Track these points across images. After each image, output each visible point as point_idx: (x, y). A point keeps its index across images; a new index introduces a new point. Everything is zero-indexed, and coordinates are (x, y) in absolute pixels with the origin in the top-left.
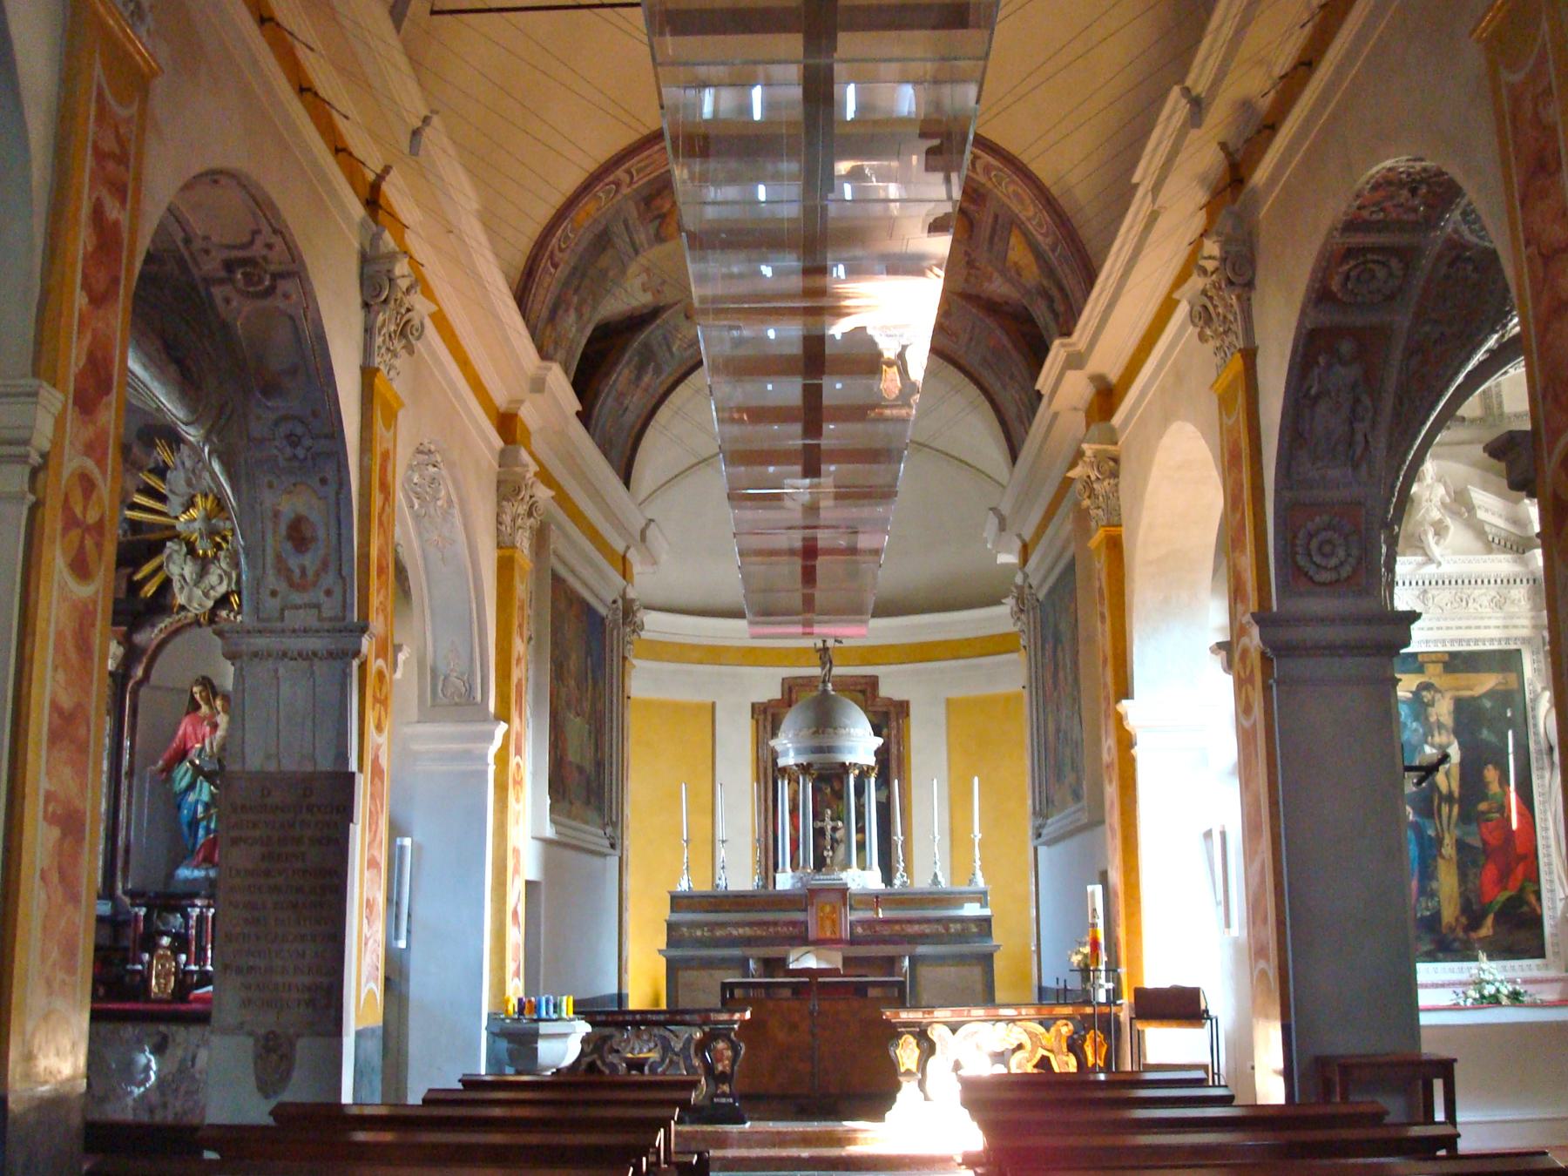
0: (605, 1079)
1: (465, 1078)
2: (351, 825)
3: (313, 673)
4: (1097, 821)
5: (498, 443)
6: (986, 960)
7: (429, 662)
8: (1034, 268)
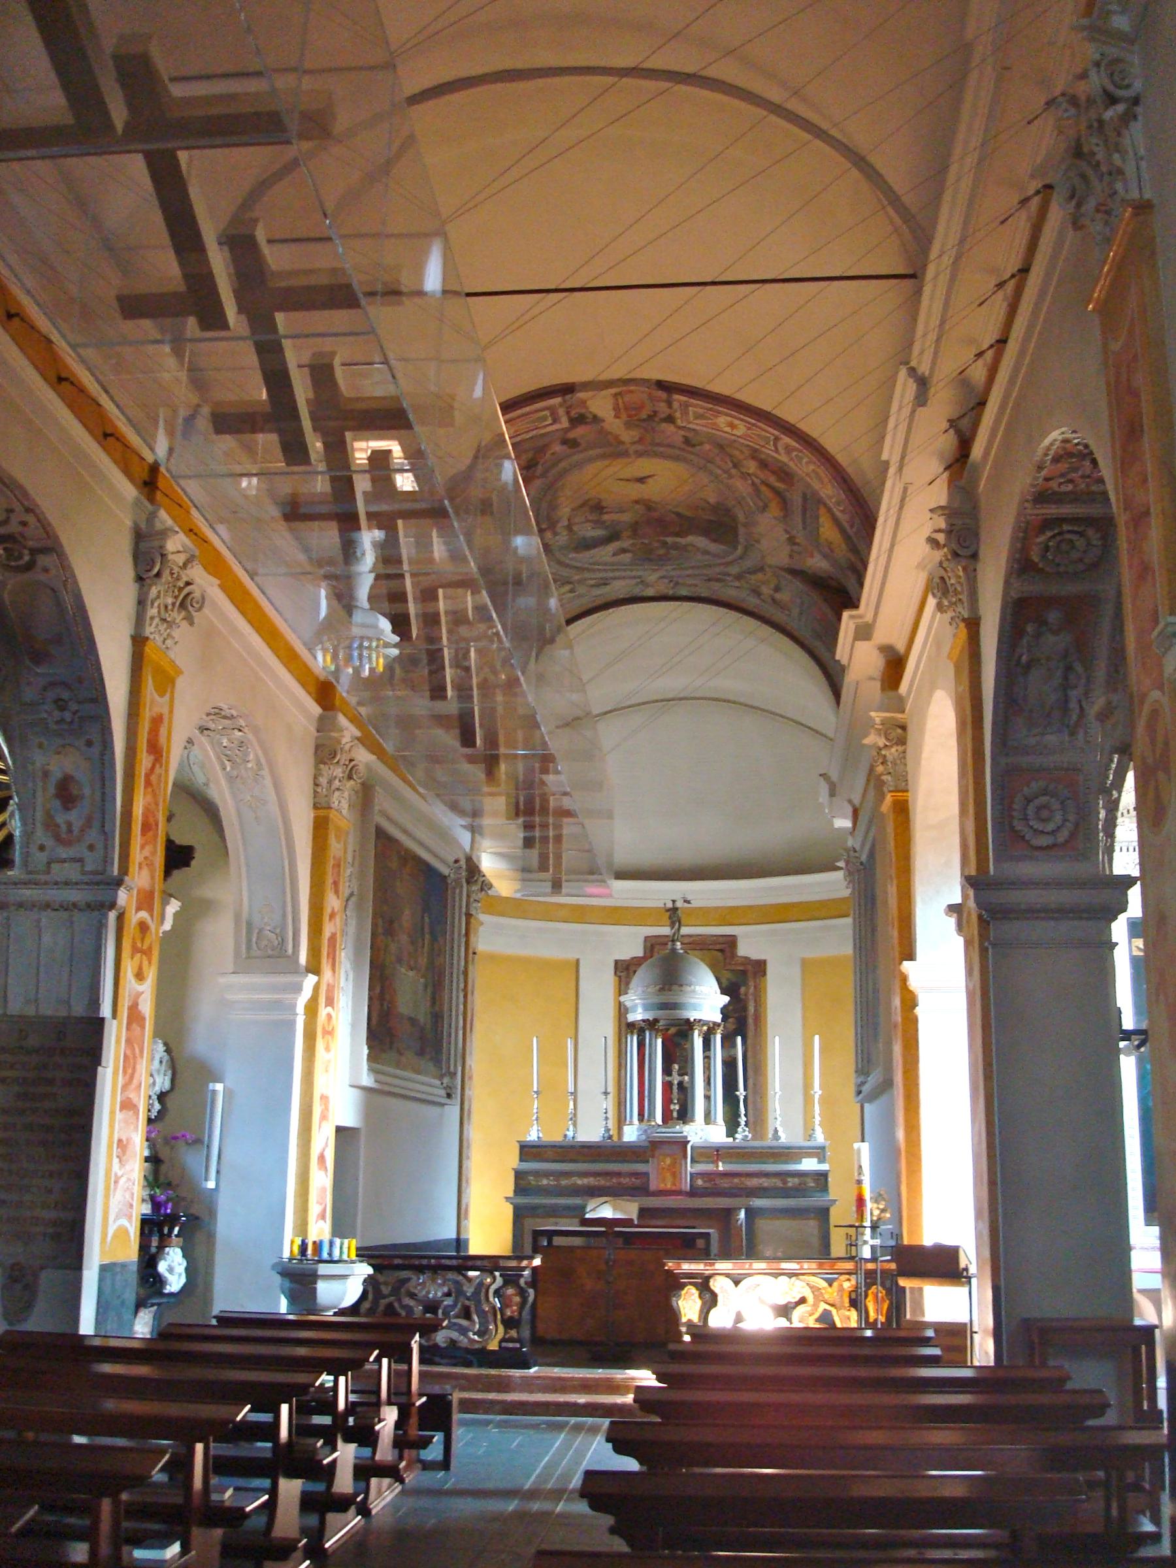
0: (401, 1321)
1: (222, 1315)
2: (100, 1069)
3: (72, 923)
4: (887, 1084)
5: (316, 710)
6: (823, 1214)
7: (245, 915)
8: (844, 546)
